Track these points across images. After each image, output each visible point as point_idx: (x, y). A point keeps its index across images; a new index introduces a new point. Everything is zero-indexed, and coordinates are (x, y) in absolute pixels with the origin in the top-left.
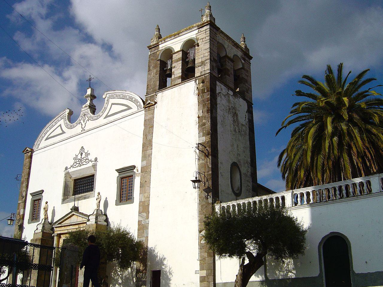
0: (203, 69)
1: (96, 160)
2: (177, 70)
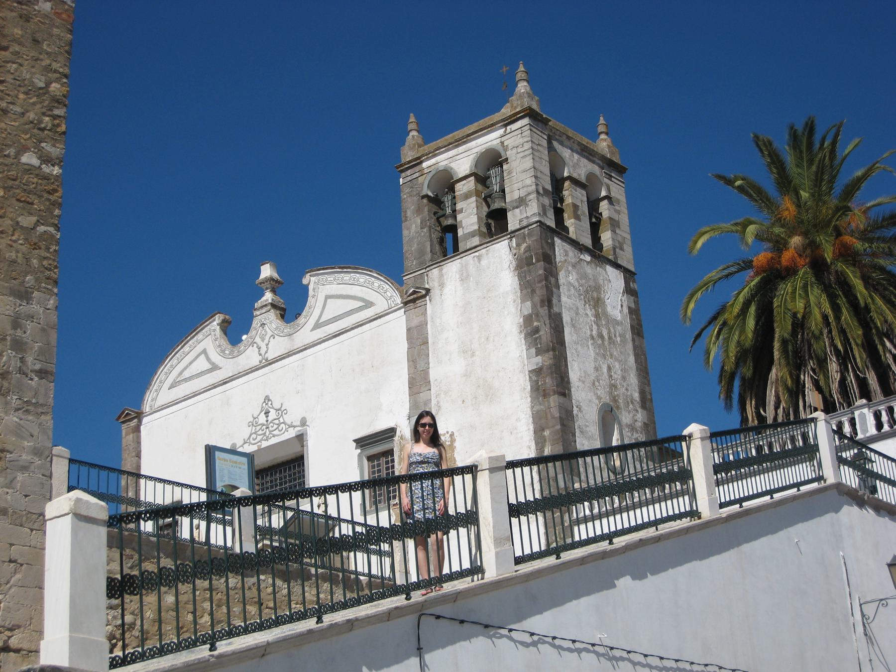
1: (304, 422)
2: (469, 218)
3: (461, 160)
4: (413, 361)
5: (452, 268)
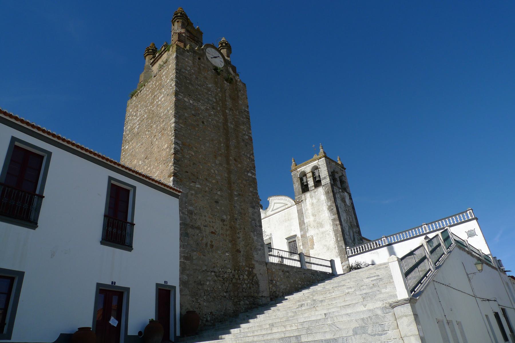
0: (326, 180)
1: (271, 234)
2: (311, 183)
3: (307, 168)
4: (300, 219)
5: (308, 194)
